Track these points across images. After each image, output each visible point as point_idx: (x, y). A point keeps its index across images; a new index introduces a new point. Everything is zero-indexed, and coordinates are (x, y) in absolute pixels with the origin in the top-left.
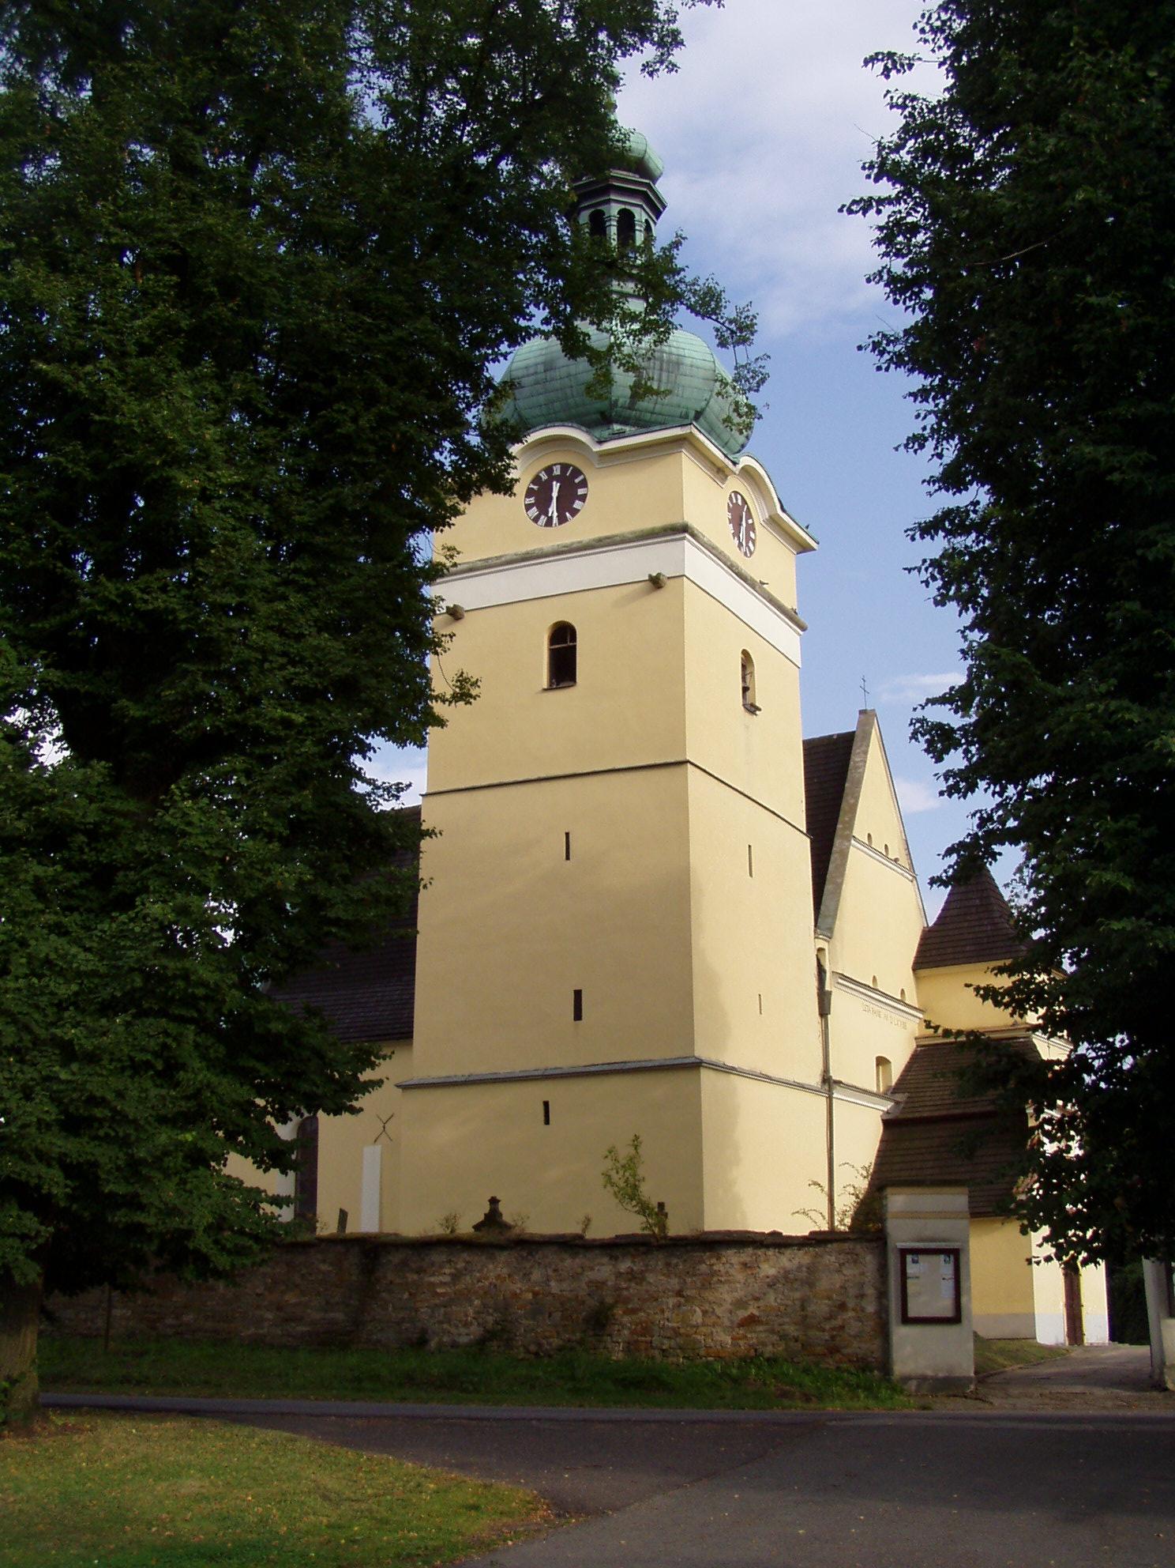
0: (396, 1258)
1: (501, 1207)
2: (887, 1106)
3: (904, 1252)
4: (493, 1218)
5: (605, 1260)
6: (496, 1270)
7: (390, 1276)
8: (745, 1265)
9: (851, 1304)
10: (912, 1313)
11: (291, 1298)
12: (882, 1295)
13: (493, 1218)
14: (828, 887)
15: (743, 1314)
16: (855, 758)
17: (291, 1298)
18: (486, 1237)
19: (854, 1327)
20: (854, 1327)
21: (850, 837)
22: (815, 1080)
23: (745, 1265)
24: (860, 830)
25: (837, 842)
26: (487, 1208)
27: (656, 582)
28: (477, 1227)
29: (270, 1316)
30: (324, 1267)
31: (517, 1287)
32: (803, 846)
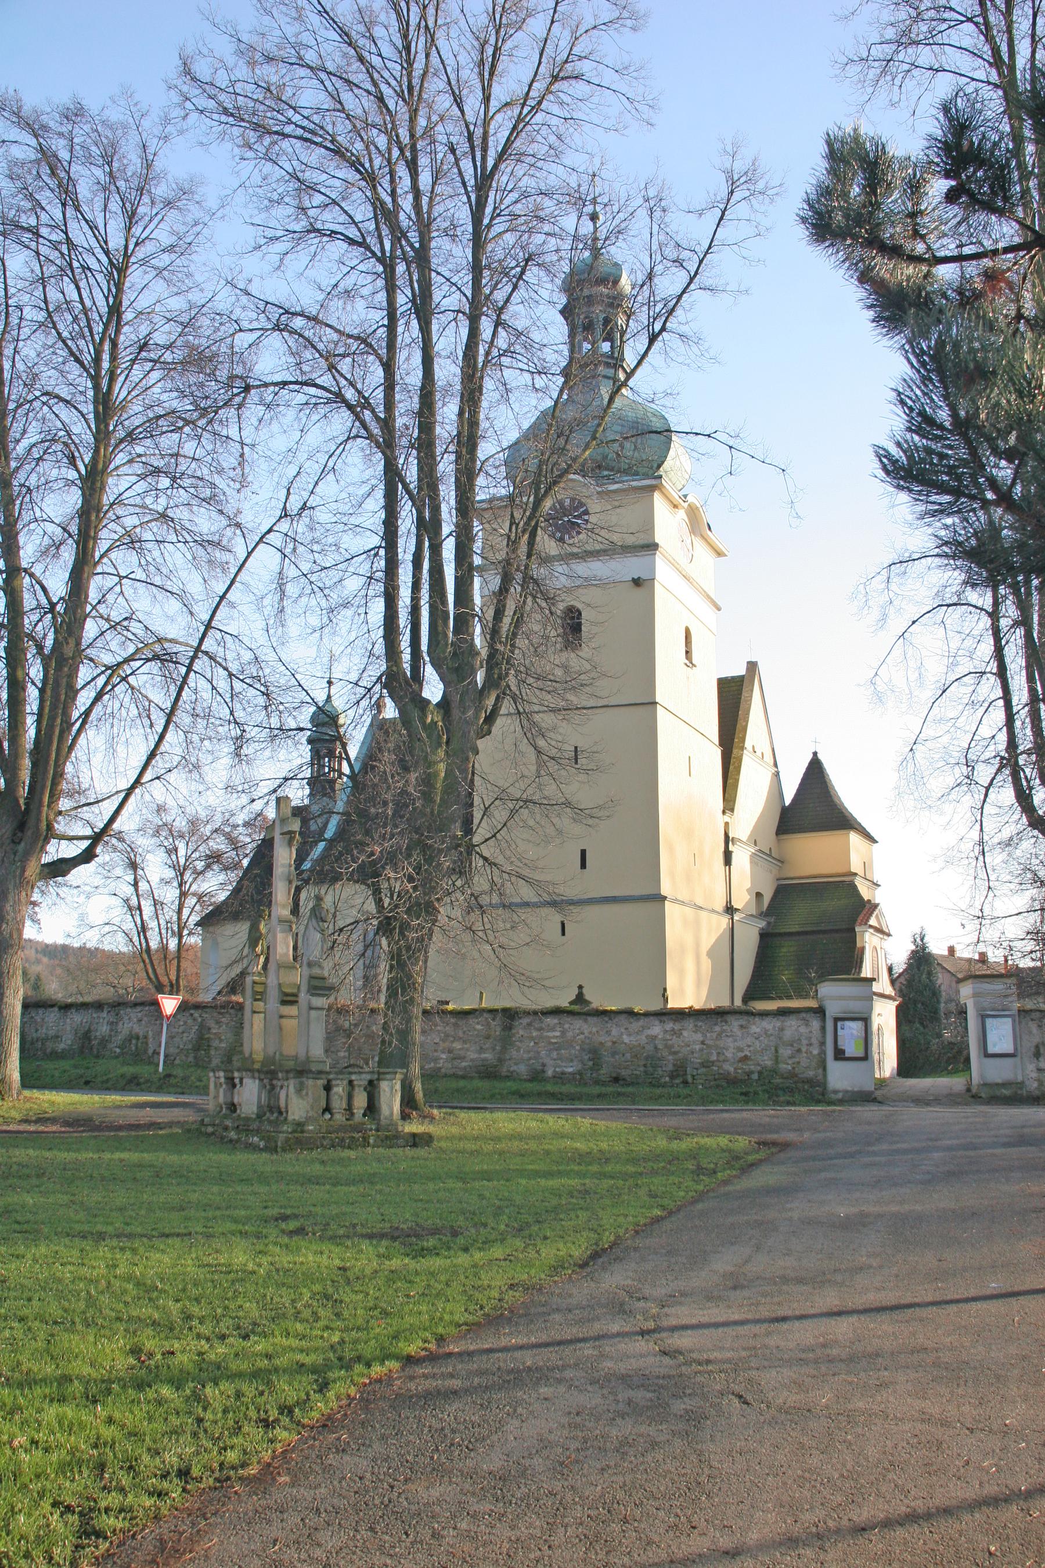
0: (525, 1021)
1: (584, 991)
2: (762, 924)
3: (836, 1020)
4: (580, 998)
5: (657, 1022)
6: (581, 1029)
7: (521, 1032)
8: (742, 1026)
9: (804, 1049)
10: (991, 1050)
11: (457, 1045)
12: (823, 1043)
13: (580, 998)
14: (730, 781)
15: (741, 1055)
16: (745, 694)
17: (457, 1045)
18: (576, 1008)
19: (804, 1063)
20: (804, 1063)
21: (743, 748)
22: (720, 904)
23: (742, 1026)
24: (748, 744)
25: (735, 751)
26: (576, 991)
27: (637, 582)
28: (571, 1003)
29: (444, 1056)
30: (479, 1027)
31: (602, 1039)
32: (717, 753)
